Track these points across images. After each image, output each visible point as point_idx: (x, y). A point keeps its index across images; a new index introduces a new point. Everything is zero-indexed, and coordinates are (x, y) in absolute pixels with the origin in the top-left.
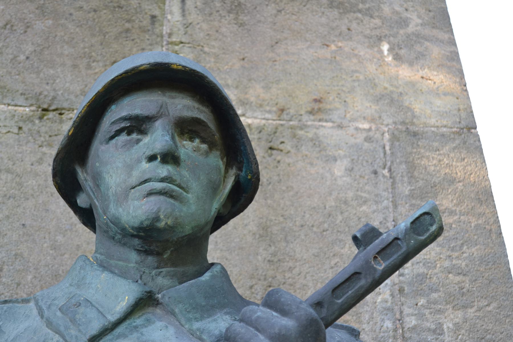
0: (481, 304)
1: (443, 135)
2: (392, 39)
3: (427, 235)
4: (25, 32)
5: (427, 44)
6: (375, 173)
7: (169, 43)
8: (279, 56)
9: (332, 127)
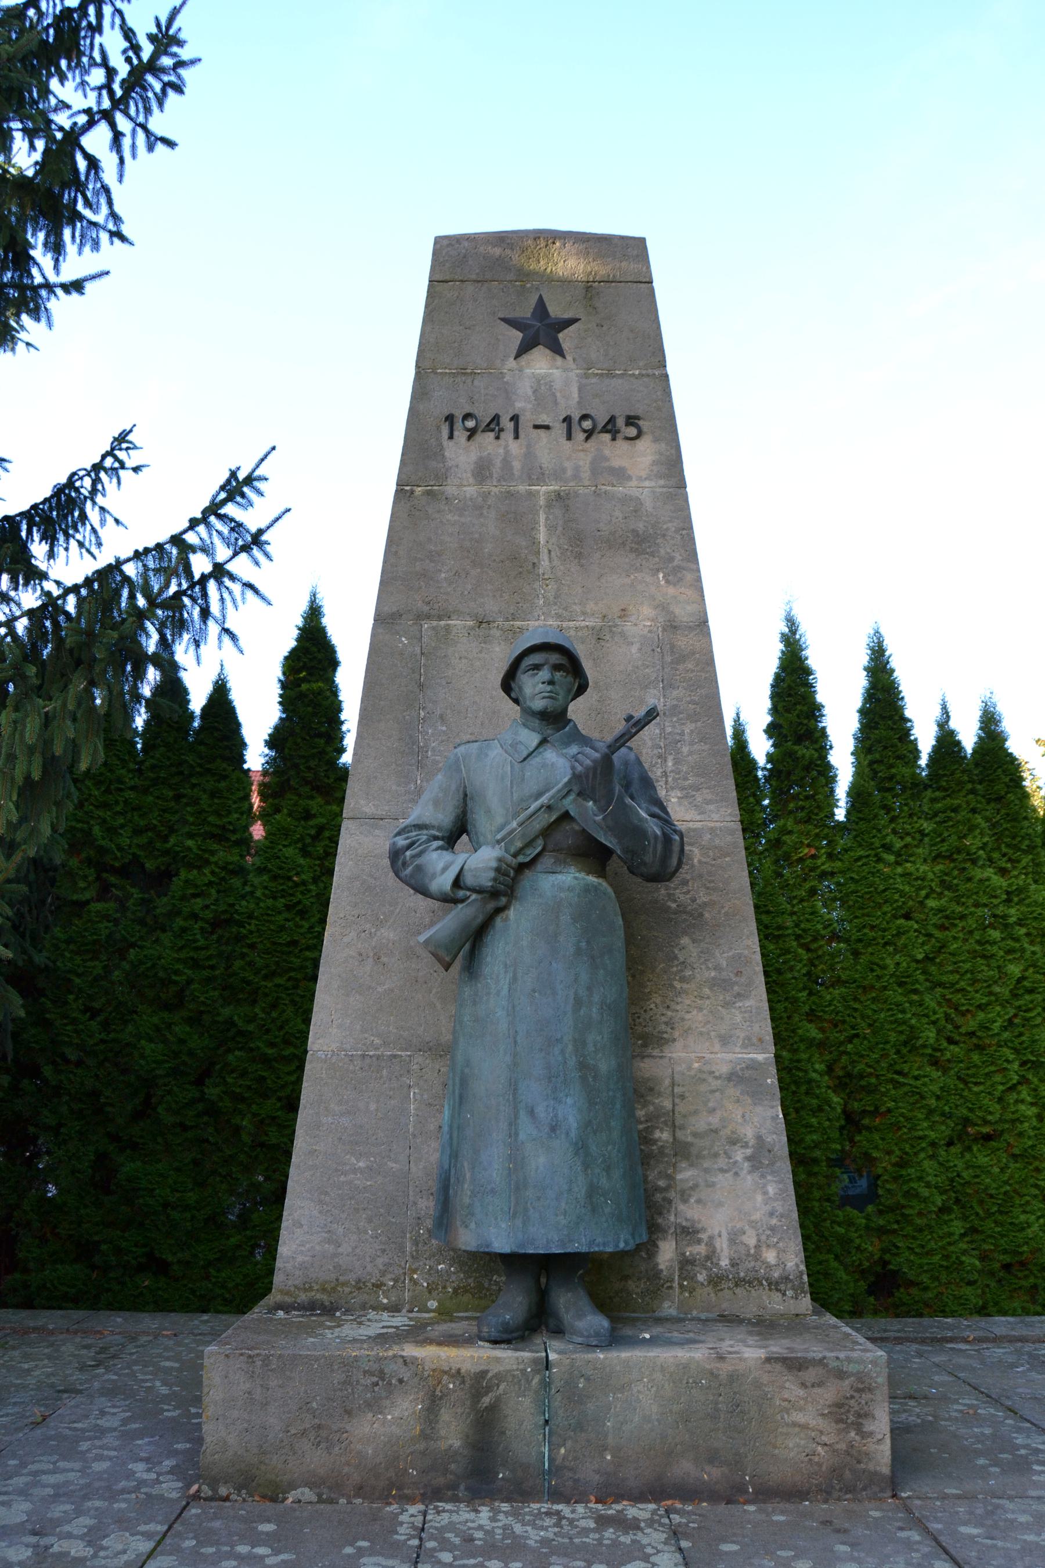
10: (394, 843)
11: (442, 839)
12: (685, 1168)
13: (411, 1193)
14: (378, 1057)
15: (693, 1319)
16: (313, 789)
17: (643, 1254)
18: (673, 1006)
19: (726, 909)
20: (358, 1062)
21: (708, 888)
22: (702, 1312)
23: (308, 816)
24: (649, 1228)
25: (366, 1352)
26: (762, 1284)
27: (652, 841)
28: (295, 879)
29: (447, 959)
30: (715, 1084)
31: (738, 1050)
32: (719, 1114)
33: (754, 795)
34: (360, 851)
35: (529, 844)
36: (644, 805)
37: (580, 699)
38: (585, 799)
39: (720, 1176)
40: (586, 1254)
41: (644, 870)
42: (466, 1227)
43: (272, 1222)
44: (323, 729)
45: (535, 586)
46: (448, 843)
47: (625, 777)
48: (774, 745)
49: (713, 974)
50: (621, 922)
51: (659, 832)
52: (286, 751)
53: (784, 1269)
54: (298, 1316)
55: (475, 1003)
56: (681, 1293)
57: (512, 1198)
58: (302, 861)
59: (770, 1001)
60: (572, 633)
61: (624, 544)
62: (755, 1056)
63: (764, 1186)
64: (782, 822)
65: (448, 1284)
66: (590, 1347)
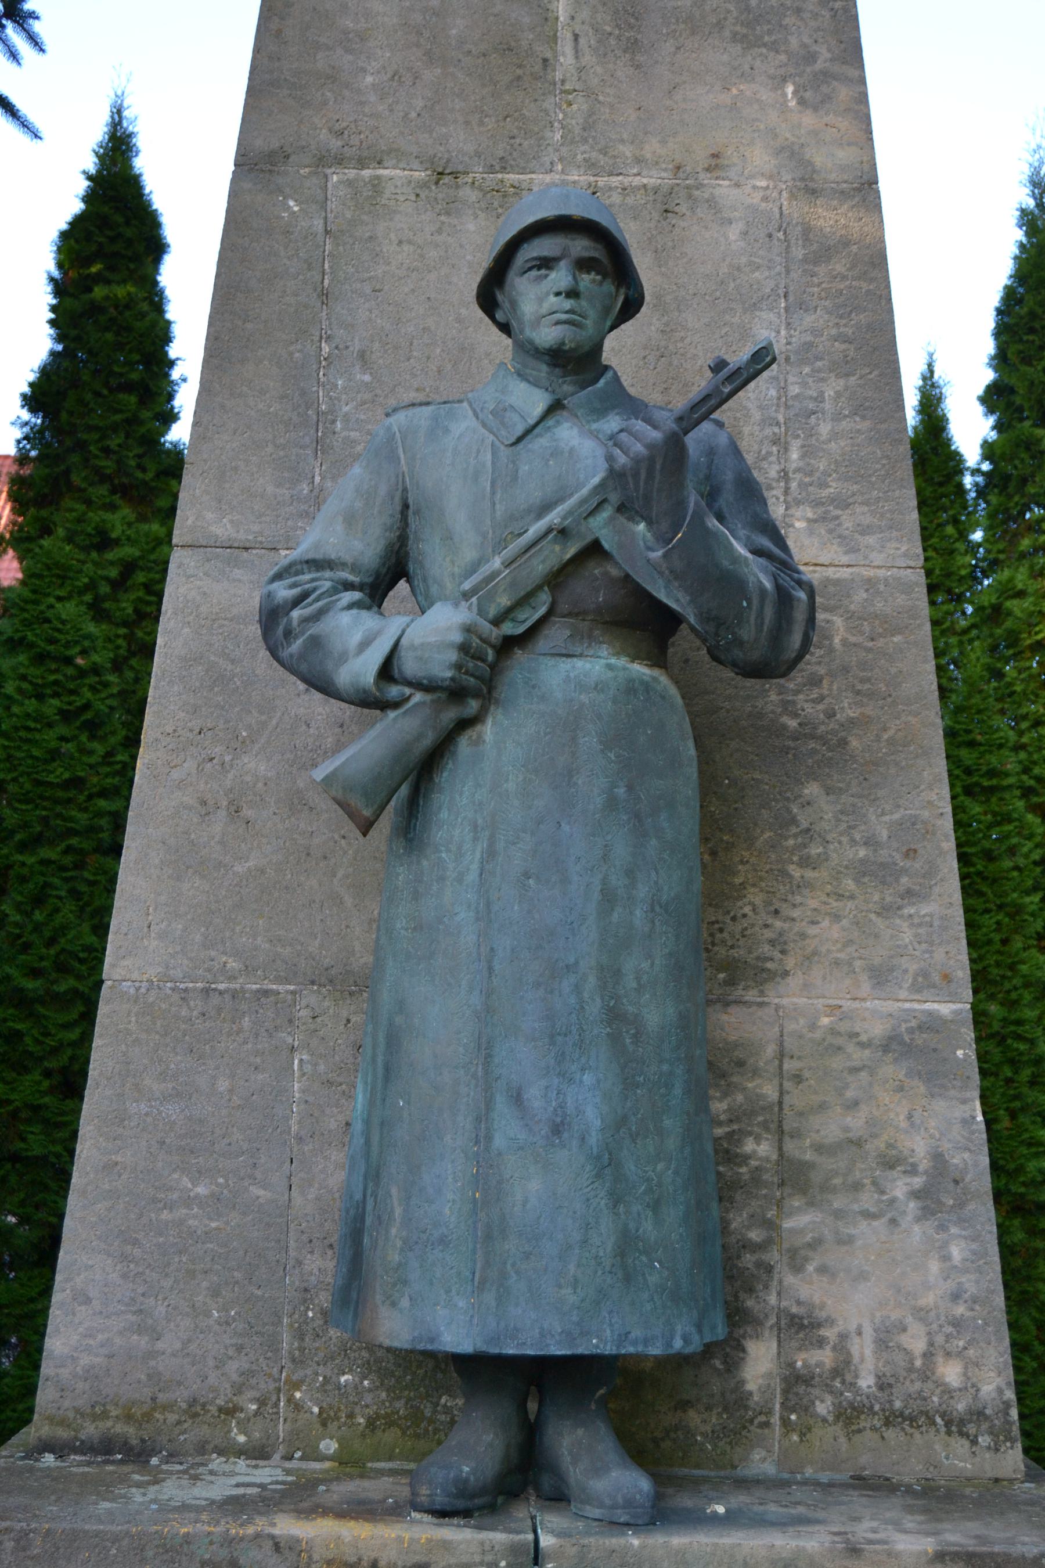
0: (863, 372)
1: (842, 192)
2: (797, 78)
3: (763, 364)
4: (414, 84)
5: (835, 83)
6: (770, 236)
7: (562, 92)
8: (677, 103)
9: (729, 186)
10: (269, 595)
11: (360, 587)
12: (799, 1208)
13: (292, 1244)
14: (234, 995)
15: (805, 1483)
16: (113, 491)
17: (718, 1363)
18: (786, 910)
19: (891, 732)
20: (197, 1004)
21: (858, 693)
22: (823, 1469)
23: (103, 541)
24: (729, 1316)
25: (207, 1528)
26: (934, 1423)
27: (755, 602)
28: (80, 661)
29: (367, 813)
30: (859, 1056)
31: (903, 994)
32: (864, 1112)
33: (956, 521)
34: (204, 609)
35: (525, 600)
36: (742, 533)
37: (627, 327)
38: (630, 519)
39: (863, 1225)
40: (615, 1358)
41: (738, 654)
42: (394, 1304)
43: (32, 1300)
44: (134, 376)
45: (546, 105)
46: (372, 596)
47: (708, 477)
48: (998, 427)
49: (862, 853)
50: (692, 752)
51: (768, 584)
52: (64, 416)
53: (975, 1397)
54: (80, 1464)
55: (416, 896)
56: (786, 1435)
57: (479, 1253)
58: (91, 628)
59: (968, 910)
60: (616, 198)
61: (720, 25)
62: (936, 1006)
63: (945, 1245)
64: (1007, 573)
65: (357, 1410)
66: (616, 1526)
